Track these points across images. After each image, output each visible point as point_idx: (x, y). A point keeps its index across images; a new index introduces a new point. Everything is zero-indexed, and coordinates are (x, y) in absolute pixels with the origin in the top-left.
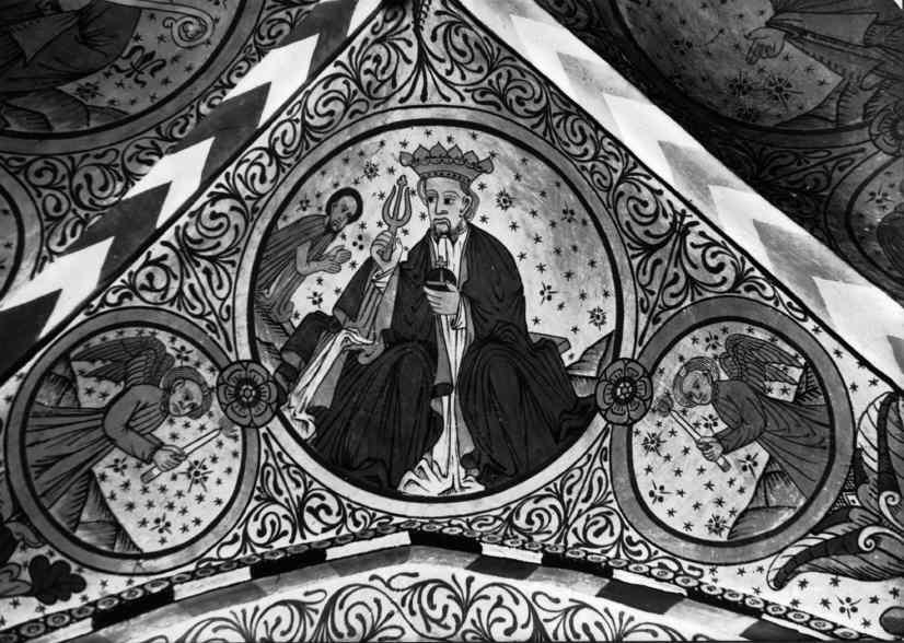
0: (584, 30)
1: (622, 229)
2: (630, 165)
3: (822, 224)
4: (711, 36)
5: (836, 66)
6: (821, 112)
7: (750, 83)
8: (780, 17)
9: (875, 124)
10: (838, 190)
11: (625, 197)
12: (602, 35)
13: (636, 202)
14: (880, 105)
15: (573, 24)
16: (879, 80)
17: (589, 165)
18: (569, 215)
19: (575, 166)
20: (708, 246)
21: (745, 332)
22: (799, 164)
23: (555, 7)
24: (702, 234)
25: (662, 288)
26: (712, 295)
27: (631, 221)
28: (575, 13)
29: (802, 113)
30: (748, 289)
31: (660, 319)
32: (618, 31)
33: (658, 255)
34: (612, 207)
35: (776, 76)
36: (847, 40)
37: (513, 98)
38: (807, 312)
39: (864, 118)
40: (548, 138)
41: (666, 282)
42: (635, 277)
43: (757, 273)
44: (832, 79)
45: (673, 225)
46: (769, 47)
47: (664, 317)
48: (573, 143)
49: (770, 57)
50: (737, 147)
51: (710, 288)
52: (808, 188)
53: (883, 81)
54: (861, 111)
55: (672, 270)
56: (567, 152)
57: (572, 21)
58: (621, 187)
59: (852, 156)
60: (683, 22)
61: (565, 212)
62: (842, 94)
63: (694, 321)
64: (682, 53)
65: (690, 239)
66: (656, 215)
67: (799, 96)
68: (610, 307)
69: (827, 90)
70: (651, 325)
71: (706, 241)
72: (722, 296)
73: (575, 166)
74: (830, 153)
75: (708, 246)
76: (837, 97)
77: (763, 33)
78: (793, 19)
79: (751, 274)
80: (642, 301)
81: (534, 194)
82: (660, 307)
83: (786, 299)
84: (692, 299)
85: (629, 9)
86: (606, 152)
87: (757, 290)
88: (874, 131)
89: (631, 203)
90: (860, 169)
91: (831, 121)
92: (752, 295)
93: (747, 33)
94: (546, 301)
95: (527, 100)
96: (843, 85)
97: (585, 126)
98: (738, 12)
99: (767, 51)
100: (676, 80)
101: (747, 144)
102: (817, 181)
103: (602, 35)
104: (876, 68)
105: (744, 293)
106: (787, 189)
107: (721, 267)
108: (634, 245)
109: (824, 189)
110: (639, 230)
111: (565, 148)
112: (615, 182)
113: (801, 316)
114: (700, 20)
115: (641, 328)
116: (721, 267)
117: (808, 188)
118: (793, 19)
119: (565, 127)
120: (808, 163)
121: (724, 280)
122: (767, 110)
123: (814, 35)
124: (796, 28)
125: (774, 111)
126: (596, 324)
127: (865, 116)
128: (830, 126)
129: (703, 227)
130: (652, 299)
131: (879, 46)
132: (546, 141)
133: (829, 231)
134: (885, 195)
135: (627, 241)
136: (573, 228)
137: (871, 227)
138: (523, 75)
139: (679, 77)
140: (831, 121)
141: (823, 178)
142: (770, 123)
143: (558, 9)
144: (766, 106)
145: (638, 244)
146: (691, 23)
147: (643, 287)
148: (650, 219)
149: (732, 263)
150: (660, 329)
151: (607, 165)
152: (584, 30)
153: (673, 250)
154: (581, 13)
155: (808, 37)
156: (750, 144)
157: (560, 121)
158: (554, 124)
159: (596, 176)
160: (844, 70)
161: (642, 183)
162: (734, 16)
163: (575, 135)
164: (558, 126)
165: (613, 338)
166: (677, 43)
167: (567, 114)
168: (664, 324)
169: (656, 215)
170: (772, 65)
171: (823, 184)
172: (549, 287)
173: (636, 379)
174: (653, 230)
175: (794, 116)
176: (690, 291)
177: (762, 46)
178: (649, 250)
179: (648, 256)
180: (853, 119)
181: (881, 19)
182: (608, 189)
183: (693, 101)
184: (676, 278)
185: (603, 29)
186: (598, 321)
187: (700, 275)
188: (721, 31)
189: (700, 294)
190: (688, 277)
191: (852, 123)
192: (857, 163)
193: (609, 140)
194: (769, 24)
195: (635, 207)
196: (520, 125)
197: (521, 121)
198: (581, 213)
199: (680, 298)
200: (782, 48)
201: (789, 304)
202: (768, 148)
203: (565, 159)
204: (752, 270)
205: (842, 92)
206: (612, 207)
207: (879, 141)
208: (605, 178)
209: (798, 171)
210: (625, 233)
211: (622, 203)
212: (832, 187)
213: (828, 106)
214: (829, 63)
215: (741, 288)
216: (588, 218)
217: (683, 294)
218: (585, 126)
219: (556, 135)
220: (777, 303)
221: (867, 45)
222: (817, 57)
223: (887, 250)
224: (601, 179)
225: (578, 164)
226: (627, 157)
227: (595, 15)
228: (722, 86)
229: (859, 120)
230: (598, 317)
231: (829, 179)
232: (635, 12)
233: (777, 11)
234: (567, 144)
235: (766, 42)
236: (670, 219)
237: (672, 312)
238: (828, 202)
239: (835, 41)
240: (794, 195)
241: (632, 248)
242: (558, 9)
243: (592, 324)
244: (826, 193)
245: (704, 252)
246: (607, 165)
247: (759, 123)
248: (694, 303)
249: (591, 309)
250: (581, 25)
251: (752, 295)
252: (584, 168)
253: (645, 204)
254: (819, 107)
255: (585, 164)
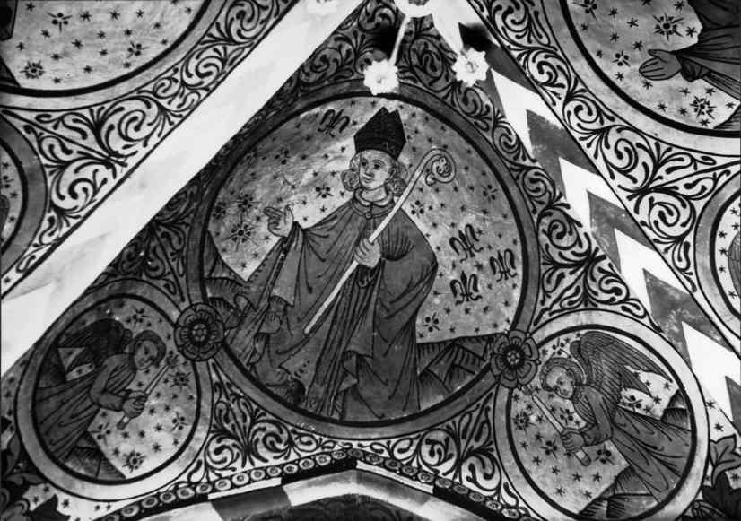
0: (298, 79)
1: (117, 103)
2: (172, 119)
3: (112, 279)
4: (290, 180)
5: (257, 276)
6: (219, 266)
7: (248, 210)
8: (301, 233)
9: (205, 307)
10: (146, 285)
11: (145, 110)
12: (294, 95)
13: (140, 119)
14: (221, 310)
15: (304, 71)
16: (242, 308)
17: (177, 76)
18: (135, 50)
19: (179, 62)
20: (94, 185)
21: (10, 215)
22: (172, 254)
23: (320, 56)
24: (105, 181)
25: (59, 137)
26: (49, 184)
27: (125, 112)
28: (316, 72)
29: (220, 252)
30: (51, 220)
31: (28, 132)
32: (299, 106)
33: (91, 137)
34: (138, 95)
35: (252, 231)
36: (276, 283)
37: (245, 8)
38: (27, 272)
39: (211, 298)
40: (206, 38)
41: (62, 140)
42: (72, 111)
43: (65, 229)
44: (245, 274)
45: (116, 154)
46: (278, 224)
47: (31, 137)
48: (199, 64)
49: (269, 225)
50: (189, 206)
51: (55, 184)
52: (149, 263)
53: (240, 311)
54: (217, 295)
55: (75, 148)
56: (191, 56)
57: (307, 70)
58: (154, 106)
59: (178, 293)
60: (304, 157)
61: (139, 46)
62: (233, 281)
63: (25, 165)
64: (277, 157)
65: (101, 168)
66: (127, 138)
67: (235, 248)
68: (44, 83)
69: (238, 270)
70: (24, 123)
71: (98, 184)
72: (47, 194)
73: (179, 62)
74: (182, 276)
75: (94, 185)
76: (231, 277)
77: (290, 220)
78: (298, 243)
79: (65, 224)
80: (49, 116)
81: (159, 15)
82: (41, 134)
83: (39, 255)
84: (48, 166)
85: (317, 115)
86: (187, 95)
87: (48, 229)
88: (198, 308)
89: (139, 115)
90: (166, 299)
91: (210, 274)
92: (45, 224)
93: (291, 207)
94: (52, 18)
95: (242, 22)
96: (240, 282)
97: (211, 78)
98: (308, 201)
99: (274, 224)
100: (252, 154)
101: (191, 212)
102: (156, 269)
103: (294, 95)
104: (252, 305)
105: (48, 215)
106: (149, 247)
107: (74, 196)
108: (102, 113)
109: (147, 275)
110: (114, 120)
111: (195, 56)
112: (160, 101)
113: (22, 267)
114: (305, 171)
115: (22, 114)
116: (74, 196)
117: (149, 263)
118: (298, 243)
119: (212, 57)
120: (174, 260)
121: (62, 198)
122: (224, 224)
123: (283, 259)
124: (289, 246)
125: (223, 229)
126: (27, 68)
127: (213, 299)
128: (206, 274)
129: (112, 183)
130: (49, 127)
131: (269, 307)
132: (204, 36)
133: (105, 285)
134: (141, 321)
135: (107, 106)
136: (124, 53)
137: (111, 314)
138: (262, 22)
139: (256, 155)
140: (210, 274)
141: (159, 273)
142: (212, 228)
143: (319, 58)
144: (227, 223)
145: (103, 117)
146: (302, 166)
147: (61, 119)
148: (124, 133)
149: (76, 208)
150: (19, 132)
151: (175, 95)
152: (298, 79)
153: (93, 151)
154: (314, 77)
155: (282, 255)
156: (192, 215)
157: (220, 54)
158: (217, 47)
159: (167, 83)
160: (252, 282)
161: (155, 129)
162: (305, 198)
163: (206, 66)
164: (216, 50)
165: (11, 85)
166: (287, 152)
167: (224, 61)
168: (24, 136)
169: (127, 138)
170: (263, 228)
171: (153, 274)
172: (66, 23)
173: (34, 43)
174: (114, 134)
175: (217, 245)
176: (54, 164)
177: (279, 219)
178: (96, 128)
179: (89, 125)
180: (211, 291)
181: (289, 309)
182: (154, 93)
183: (233, 167)
184: (68, 152)
185: (300, 95)
186: (29, 70)
187: (69, 175)
188: (294, 187)
189: (51, 173)
190: (68, 164)
191: (208, 290)
192: (172, 296)
193: (196, 100)
194: (296, 224)
195: (135, 118)
196: (220, 12)
197: (224, 13)
198: (138, 62)
199: (49, 155)
200: (276, 235)
201: (33, 257)
202: (188, 228)
203: (186, 52)
204: (68, 225)
205: (235, 281)
206: (138, 95)
207: (191, 311)
208: (164, 91)
209: (166, 256)
210: (115, 104)
211: (140, 105)
212: (151, 281)
213: (224, 271)
214: (260, 271)
215: (53, 214)
216: (132, 69)
217: (53, 158)
218: (211, 78)
219: (208, 47)
220: (36, 246)
221: (271, 298)
222: (265, 262)
223: (86, 330)
224: (164, 87)
225: (179, 66)
226: (181, 116)
227: (312, 89)
228: (247, 189)
229: (209, 295)
230: (34, 71)
231: (158, 278)
232: (314, 120)
233: (305, 231)
234: (198, 57)
235: (282, 222)
236: (121, 152)
237: (35, 145)
238: (136, 279)
239: (277, 275)
240: (142, 254)
241: (99, 111)
242: (319, 58)
243: (26, 64)
244: (144, 277)
245: (89, 181)
246: (175, 95)
247: (212, 218)
248: (43, 167)
249: (42, 64)
250: (303, 77)
251: (45, 224)
252: (176, 71)
253: (137, 128)
254: (224, 264)
255: (179, 73)
